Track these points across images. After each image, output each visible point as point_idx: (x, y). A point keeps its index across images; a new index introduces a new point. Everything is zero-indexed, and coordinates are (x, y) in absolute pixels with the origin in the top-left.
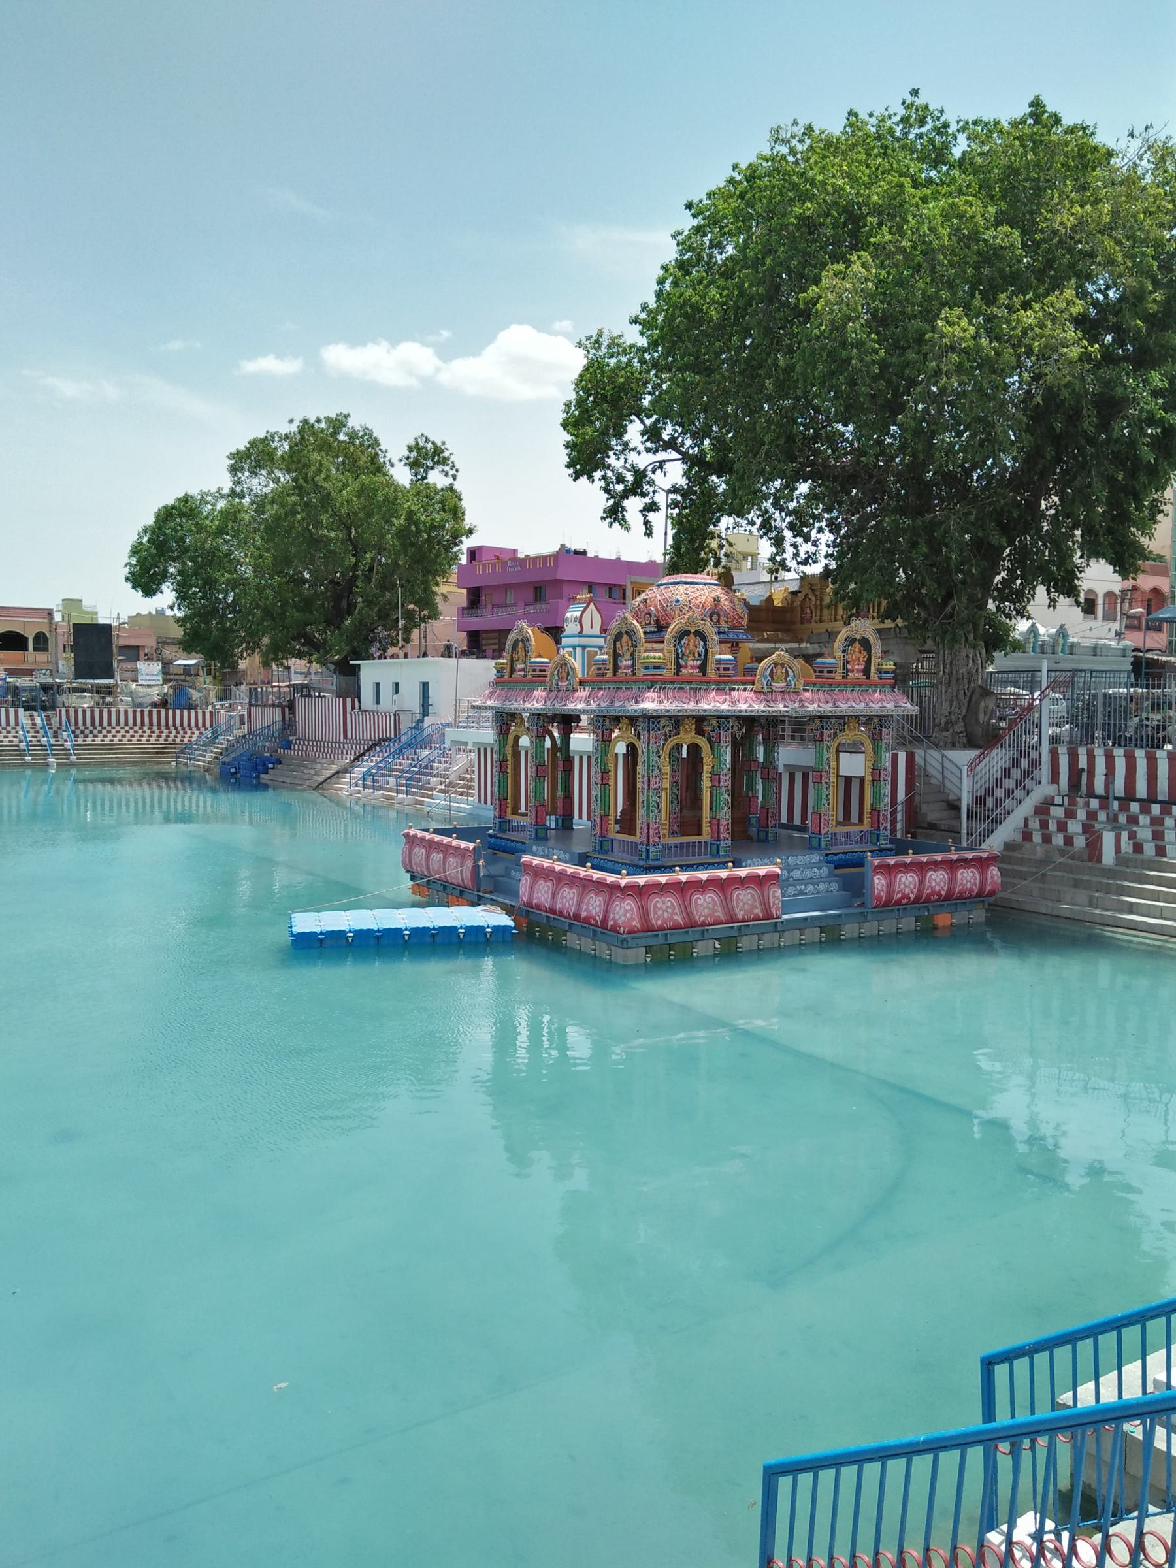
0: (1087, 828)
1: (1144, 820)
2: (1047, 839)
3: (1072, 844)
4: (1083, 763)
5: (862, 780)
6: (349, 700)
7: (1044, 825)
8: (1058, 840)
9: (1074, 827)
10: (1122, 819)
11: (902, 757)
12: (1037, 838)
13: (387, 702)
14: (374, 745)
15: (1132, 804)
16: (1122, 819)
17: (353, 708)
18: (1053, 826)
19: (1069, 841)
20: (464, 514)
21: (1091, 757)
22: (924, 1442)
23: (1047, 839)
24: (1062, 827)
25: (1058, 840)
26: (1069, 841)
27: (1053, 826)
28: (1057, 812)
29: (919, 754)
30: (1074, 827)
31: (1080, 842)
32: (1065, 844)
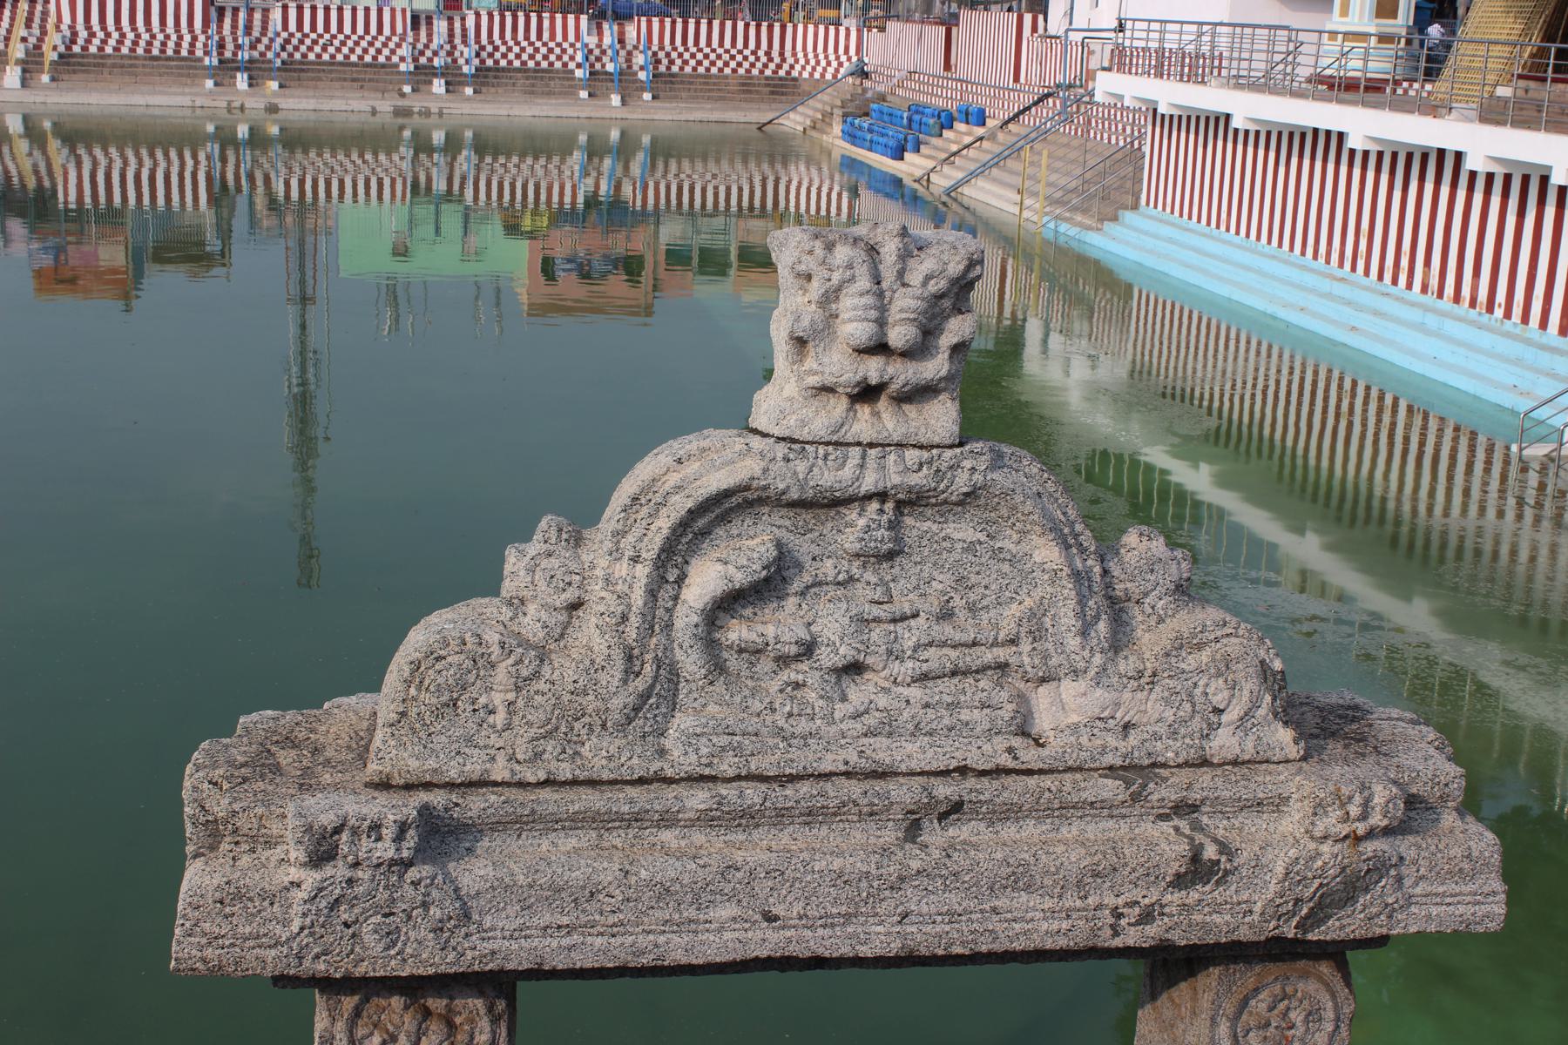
6: (1028, 18)
17: (1034, 29)
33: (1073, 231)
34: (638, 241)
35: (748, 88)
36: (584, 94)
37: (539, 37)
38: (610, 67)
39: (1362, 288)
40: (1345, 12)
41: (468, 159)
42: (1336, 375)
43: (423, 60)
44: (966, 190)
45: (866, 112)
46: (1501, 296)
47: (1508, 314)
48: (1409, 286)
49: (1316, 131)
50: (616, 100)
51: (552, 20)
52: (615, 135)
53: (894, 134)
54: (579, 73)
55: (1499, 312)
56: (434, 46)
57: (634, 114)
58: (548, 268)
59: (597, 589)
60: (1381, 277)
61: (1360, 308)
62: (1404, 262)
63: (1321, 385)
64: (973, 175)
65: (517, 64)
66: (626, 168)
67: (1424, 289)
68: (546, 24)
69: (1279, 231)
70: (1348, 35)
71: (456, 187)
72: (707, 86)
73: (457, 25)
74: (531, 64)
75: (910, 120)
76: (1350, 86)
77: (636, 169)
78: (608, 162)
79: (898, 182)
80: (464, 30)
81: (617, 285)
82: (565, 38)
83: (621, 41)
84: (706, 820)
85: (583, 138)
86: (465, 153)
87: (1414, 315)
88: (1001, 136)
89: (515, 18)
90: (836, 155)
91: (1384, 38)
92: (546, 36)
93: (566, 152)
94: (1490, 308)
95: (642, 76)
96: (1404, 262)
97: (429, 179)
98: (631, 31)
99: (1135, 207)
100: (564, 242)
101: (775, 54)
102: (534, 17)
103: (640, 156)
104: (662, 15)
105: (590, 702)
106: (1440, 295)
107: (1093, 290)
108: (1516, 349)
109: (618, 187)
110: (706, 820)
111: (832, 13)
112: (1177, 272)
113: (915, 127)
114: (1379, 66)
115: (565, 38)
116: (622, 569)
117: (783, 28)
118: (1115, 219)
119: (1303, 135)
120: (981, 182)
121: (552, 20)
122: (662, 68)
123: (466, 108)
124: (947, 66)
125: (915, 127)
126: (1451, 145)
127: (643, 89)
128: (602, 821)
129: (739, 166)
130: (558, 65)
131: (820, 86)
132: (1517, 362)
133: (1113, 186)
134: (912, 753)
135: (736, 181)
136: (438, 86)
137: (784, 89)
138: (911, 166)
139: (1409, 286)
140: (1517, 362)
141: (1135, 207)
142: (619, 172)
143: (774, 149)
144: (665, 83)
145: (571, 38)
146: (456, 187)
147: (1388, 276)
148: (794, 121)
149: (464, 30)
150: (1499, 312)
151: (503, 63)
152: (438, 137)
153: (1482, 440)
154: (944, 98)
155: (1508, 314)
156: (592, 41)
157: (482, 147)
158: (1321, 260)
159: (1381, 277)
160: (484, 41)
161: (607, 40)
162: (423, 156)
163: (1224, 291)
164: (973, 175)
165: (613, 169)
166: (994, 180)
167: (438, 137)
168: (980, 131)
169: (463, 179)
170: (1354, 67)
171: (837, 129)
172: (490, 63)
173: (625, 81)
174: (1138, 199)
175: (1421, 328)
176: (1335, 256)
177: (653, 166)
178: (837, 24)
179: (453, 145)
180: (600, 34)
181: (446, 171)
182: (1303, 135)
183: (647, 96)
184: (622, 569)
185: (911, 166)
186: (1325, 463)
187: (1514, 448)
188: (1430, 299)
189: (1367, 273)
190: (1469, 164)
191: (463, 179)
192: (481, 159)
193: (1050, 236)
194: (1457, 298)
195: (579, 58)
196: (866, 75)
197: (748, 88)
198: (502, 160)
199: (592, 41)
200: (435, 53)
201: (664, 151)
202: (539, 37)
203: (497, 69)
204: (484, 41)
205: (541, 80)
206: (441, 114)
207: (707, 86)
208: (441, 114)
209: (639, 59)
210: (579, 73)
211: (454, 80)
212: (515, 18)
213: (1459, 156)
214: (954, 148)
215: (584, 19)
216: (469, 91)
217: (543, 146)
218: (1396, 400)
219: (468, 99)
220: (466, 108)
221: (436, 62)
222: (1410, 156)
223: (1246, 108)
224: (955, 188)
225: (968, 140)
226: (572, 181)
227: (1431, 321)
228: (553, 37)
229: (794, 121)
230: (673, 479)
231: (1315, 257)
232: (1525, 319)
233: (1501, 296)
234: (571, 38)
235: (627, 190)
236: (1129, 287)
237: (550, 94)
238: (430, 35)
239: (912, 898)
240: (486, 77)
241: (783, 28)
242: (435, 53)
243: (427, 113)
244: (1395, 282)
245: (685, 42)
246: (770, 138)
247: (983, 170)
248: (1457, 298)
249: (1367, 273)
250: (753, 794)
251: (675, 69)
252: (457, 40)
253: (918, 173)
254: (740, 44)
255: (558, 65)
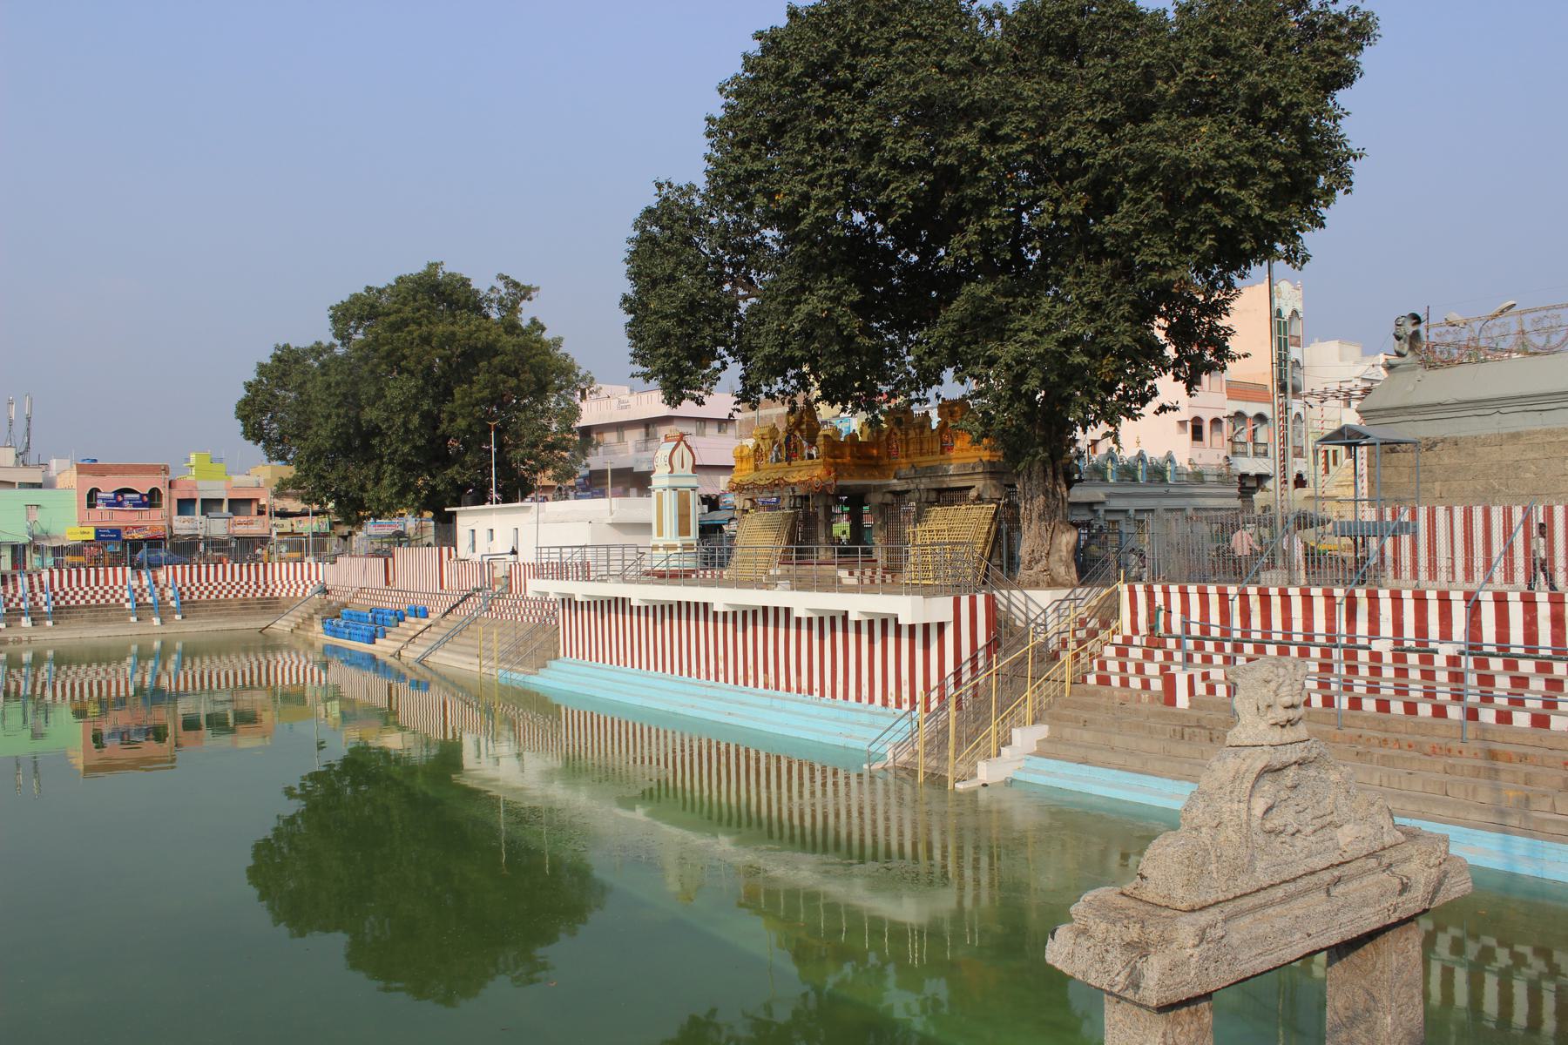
0: (1164, 669)
1: (1218, 659)
2: (1125, 682)
3: (1416, 713)
4: (1159, 599)
5: (941, 626)
6: (445, 549)
7: (1123, 667)
8: (1135, 683)
9: (1152, 669)
10: (1197, 658)
11: (981, 600)
12: (1115, 681)
13: (483, 546)
14: (468, 596)
15: (1268, 647)
16: (1197, 658)
17: (450, 556)
18: (1131, 668)
19: (1146, 684)
20: (465, 283)
21: (1166, 593)
22: (545, 499)
23: (1125, 682)
24: (1140, 669)
25: (1135, 683)
26: (1146, 684)
27: (1131, 668)
28: (1135, 653)
29: (1000, 596)
30: (1152, 669)
31: (1157, 685)
32: (1379, 709)
33: (520, 677)
34: (161, 715)
35: (246, 606)
36: (133, 619)
37: (97, 583)
38: (150, 600)
39: (725, 689)
40: (660, 533)
41: (49, 671)
42: (714, 743)
43: (12, 605)
44: (430, 659)
45: (334, 614)
46: (816, 684)
47: (822, 694)
48: (756, 685)
49: (679, 603)
50: (156, 621)
51: (106, 572)
52: (157, 645)
53: (366, 628)
54: (128, 605)
55: (816, 694)
56: (20, 594)
57: (170, 630)
58: (98, 739)
59: (1226, 817)
60: (736, 682)
61: (730, 702)
62: (751, 672)
63: (705, 752)
64: (432, 649)
65: (83, 602)
66: (164, 667)
67: (766, 686)
68: (101, 574)
69: (662, 663)
70: (666, 547)
71: (38, 690)
72: (219, 607)
73: (36, 579)
74: (93, 602)
75: (374, 618)
76: (662, 575)
77: (171, 667)
78: (151, 663)
79: (373, 658)
80: (41, 583)
81: (150, 748)
82: (115, 582)
83: (156, 582)
84: (1283, 901)
85: (134, 648)
86: (46, 666)
87: (767, 702)
88: (443, 623)
89: (79, 572)
90: (318, 645)
91: (685, 547)
92: (102, 583)
93: (121, 660)
94: (811, 692)
95: (173, 604)
96: (751, 672)
97: (18, 686)
98: (161, 575)
99: (557, 658)
100: (119, 719)
101: (261, 582)
102: (92, 571)
103: (175, 657)
104: (174, 564)
105: (1239, 862)
106: (777, 688)
107: (534, 712)
108: (834, 713)
109: (158, 677)
110: (1283, 901)
111: (297, 555)
112: (600, 694)
113: (378, 623)
114: (690, 563)
115: (115, 582)
116: (1235, 806)
117: (265, 566)
118: (545, 666)
119: (671, 607)
120: (439, 653)
121: (106, 572)
122: (186, 598)
123: (48, 635)
124: (387, 583)
125: (378, 623)
126: (782, 604)
127: (175, 613)
128: (1253, 909)
129: (242, 657)
130: (113, 601)
131: (293, 602)
132: (836, 719)
133: (539, 644)
134: (1318, 862)
135: (241, 665)
136: (26, 622)
137: (270, 605)
138: (383, 648)
139: (756, 685)
140: (836, 719)
141: (557, 658)
142: (159, 668)
143: (269, 644)
144: (189, 607)
145: (120, 582)
146: (38, 690)
147: (741, 682)
148: (282, 626)
149: (41, 583)
150: (816, 694)
151: (73, 603)
152: (27, 657)
153: (817, 766)
154: (390, 603)
155: (822, 694)
156: (135, 584)
157: (61, 660)
158: (694, 677)
159: (736, 682)
160: (57, 589)
161: (146, 582)
162: (14, 671)
163: (637, 702)
164: (432, 649)
165: (154, 669)
166: (449, 651)
167: (27, 657)
168: (427, 622)
169: (44, 685)
170: (674, 564)
171: (318, 627)
172: (63, 603)
173: (162, 609)
174: (557, 652)
175: (771, 708)
176: (703, 674)
177: (183, 664)
178: (302, 561)
179: (38, 660)
180: (140, 578)
181: (31, 679)
182: (671, 607)
183: (178, 617)
184: (1235, 806)
185: (383, 648)
186: (724, 799)
187: (866, 766)
188: (771, 691)
189: (726, 681)
190: (795, 614)
191: (44, 685)
192: (59, 668)
193: (503, 682)
194: (788, 689)
195: (127, 595)
196: (327, 592)
197: (246, 606)
198: (74, 668)
199: (135, 584)
200: (21, 600)
201: (191, 652)
202: (97, 583)
203: (68, 607)
204: (57, 589)
205: (101, 612)
206: (29, 641)
207: (219, 607)
208: (29, 641)
209: (170, 593)
210: (128, 605)
211: (37, 617)
212: (79, 572)
213: (787, 610)
214: (412, 633)
215: (128, 569)
216: (49, 623)
217: (102, 656)
218: (757, 752)
219: (49, 629)
220: (48, 635)
221: (22, 605)
222: (745, 613)
223: (639, 594)
224: (424, 656)
225: (421, 628)
226: (125, 678)
227: (776, 703)
228: (106, 583)
229: (282, 626)
230: (1244, 767)
231: (690, 674)
232: (834, 695)
233: (816, 684)
234: (120, 582)
235: (164, 682)
236: (558, 706)
237: (109, 621)
238: (16, 588)
239: (1343, 918)
240: (61, 613)
241: (265, 566)
242: (21, 600)
243: (20, 641)
244: (746, 684)
245: (199, 579)
246: (267, 637)
247: (439, 645)
248: (788, 689)
249: (726, 681)
250: (1291, 887)
251: (195, 598)
252: (37, 590)
253: (392, 651)
254: (228, 578)
255: (113, 601)
